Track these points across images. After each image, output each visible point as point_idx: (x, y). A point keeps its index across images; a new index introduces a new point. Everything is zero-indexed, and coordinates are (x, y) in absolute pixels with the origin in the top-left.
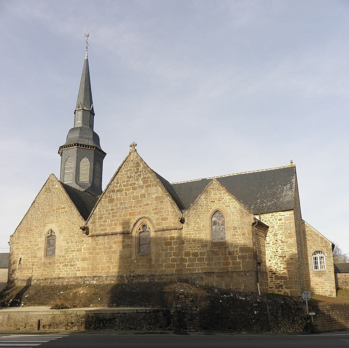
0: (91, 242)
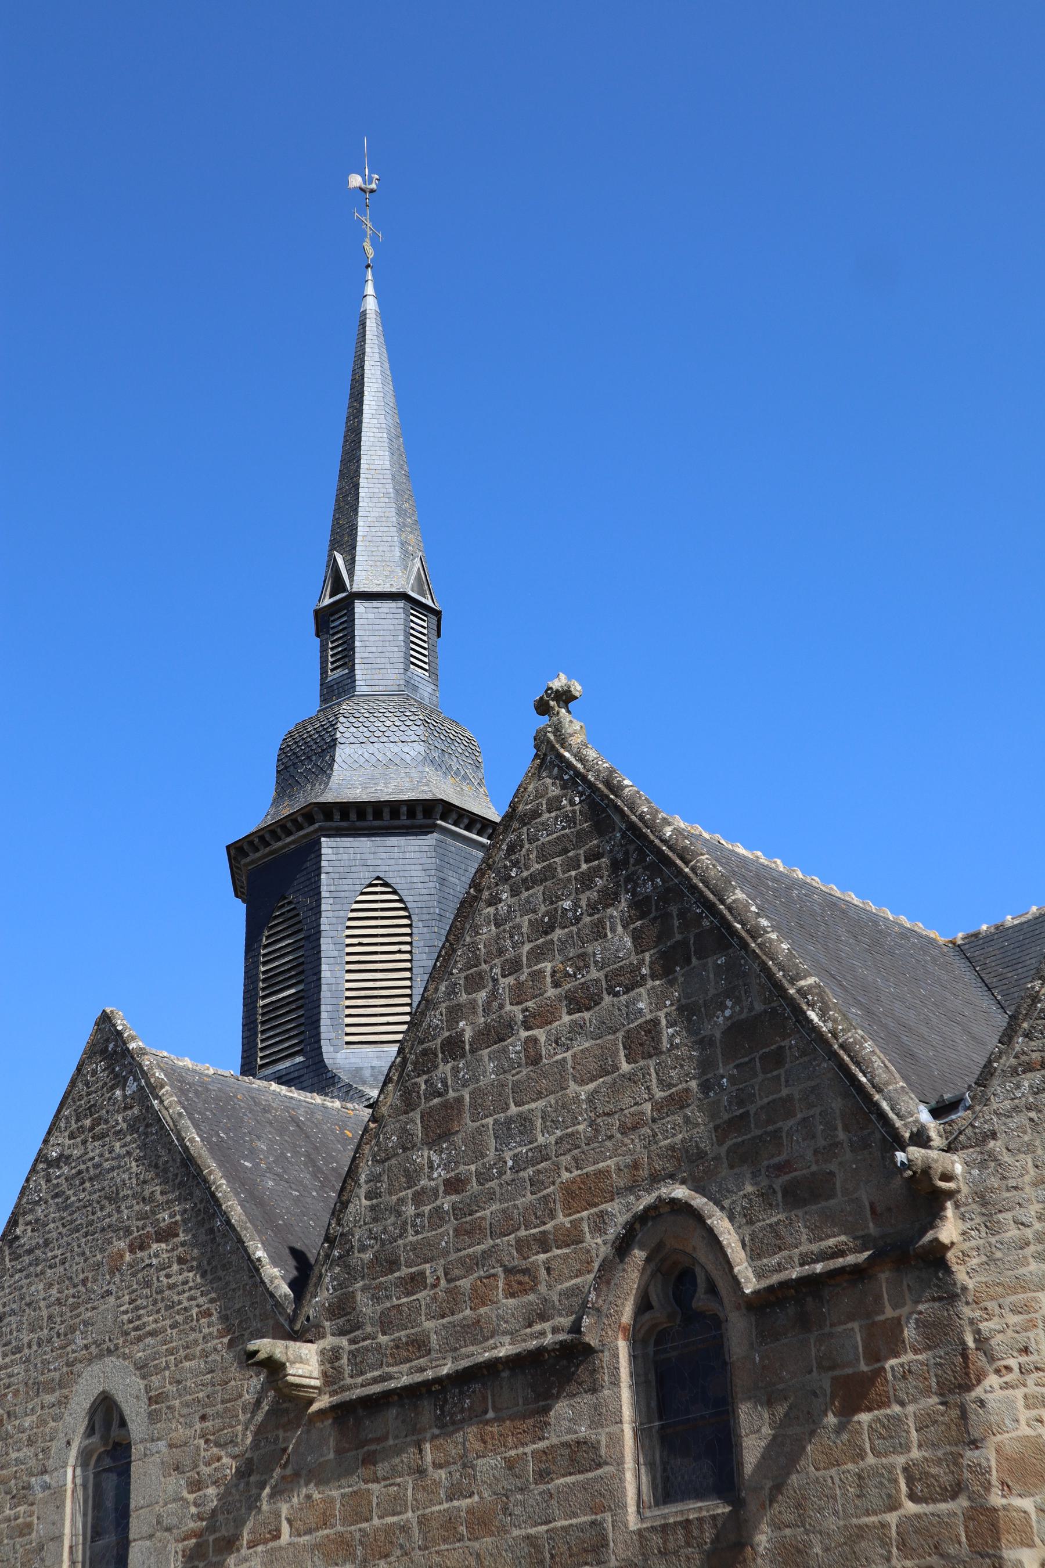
0: (332, 1456)
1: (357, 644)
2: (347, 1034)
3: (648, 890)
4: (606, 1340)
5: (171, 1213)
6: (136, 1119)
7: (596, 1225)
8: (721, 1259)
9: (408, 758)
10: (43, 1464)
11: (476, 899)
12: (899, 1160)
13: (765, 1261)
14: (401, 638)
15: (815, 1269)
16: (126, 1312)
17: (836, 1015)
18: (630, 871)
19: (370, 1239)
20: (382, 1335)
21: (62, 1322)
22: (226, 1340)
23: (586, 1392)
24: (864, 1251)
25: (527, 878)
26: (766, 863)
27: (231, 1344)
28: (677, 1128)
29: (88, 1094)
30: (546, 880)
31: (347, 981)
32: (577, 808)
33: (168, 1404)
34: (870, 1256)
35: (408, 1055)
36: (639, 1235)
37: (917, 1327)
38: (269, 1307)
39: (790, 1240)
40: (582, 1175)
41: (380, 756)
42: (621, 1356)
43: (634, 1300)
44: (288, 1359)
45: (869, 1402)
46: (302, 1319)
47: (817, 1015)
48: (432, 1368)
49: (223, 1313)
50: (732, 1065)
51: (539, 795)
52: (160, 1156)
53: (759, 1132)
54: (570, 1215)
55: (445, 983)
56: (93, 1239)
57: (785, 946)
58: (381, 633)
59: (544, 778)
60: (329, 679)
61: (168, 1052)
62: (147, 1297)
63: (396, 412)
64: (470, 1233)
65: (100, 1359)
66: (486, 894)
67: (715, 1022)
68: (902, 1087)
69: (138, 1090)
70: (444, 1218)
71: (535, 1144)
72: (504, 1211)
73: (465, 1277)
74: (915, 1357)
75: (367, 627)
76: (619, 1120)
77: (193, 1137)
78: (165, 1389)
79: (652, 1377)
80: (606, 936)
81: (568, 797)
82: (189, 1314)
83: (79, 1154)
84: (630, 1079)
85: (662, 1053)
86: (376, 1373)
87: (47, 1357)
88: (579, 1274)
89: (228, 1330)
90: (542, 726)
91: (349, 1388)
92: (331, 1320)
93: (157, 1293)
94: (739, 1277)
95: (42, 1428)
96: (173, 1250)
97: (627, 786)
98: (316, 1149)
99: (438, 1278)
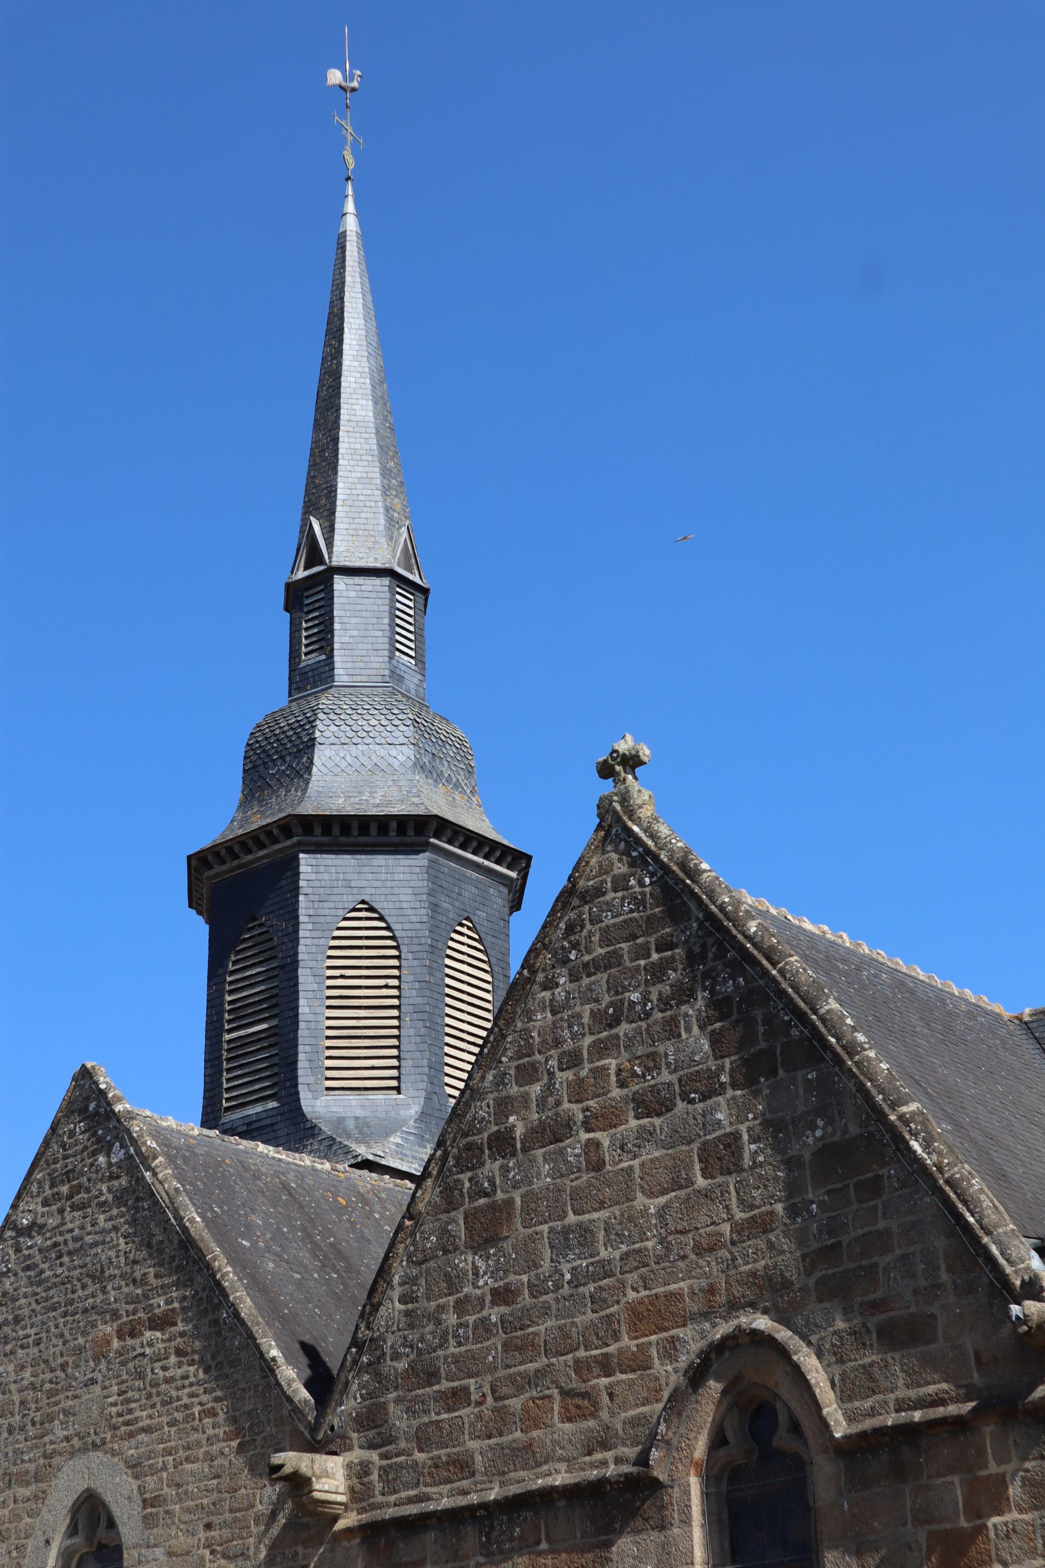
1: (336, 626)
2: (327, 1079)
3: (729, 990)
4: (676, 1476)
5: (167, 1300)
6: (124, 1191)
7: (666, 1351)
8: (807, 1398)
9: (396, 764)
10: (18, 1563)
11: (530, 981)
12: (822, 1122)
13: (857, 1404)
14: (386, 621)
15: (913, 1416)
16: (115, 1404)
17: (942, 1147)
18: (708, 967)
19: (405, 1346)
20: (419, 1452)
21: (38, 1410)
22: (234, 1444)
23: (653, 1529)
24: (968, 1401)
25: (588, 963)
26: (833, 938)
27: (241, 1449)
28: (759, 1253)
29: (65, 1157)
30: (611, 967)
31: (328, 1018)
32: (647, 889)
33: (167, 1508)
34: (974, 1409)
35: (449, 1149)
36: (715, 1366)
37: (1024, 1485)
38: (285, 1412)
39: (884, 1384)
40: (651, 1295)
41: (365, 760)
42: (693, 1493)
43: (709, 1435)
44: (314, 1474)
45: (968, 1560)
46: (325, 1427)
47: (921, 1145)
48: (476, 1491)
49: (231, 1413)
50: (822, 1191)
51: (604, 870)
52: (153, 1235)
53: (852, 1266)
54: (636, 1338)
55: (493, 1072)
56: (74, 1321)
57: (884, 1066)
58: (364, 614)
59: (608, 852)
60: (303, 664)
61: (151, 1111)
62: (139, 1390)
63: (380, 353)
64: (521, 1349)
65: (84, 1454)
66: (540, 977)
67: (805, 1142)
68: (1013, 1230)
69: (126, 1159)
70: (491, 1331)
71: (597, 1258)
72: (561, 1328)
73: (516, 1396)
74: (1020, 1517)
75: (347, 607)
76: (693, 1239)
77: (194, 1218)
78: (162, 1492)
79: (725, 1516)
80: (679, 1035)
81: (637, 877)
82: (190, 1412)
83: (55, 1224)
84: (706, 1196)
85: (743, 1170)
86: (412, 1493)
87: (21, 1446)
88: (646, 1402)
89: (237, 1433)
90: (606, 793)
91: (380, 1506)
92: (358, 1431)
93: (151, 1386)
94: (828, 1420)
95: (16, 1524)
96: (170, 1340)
97: (705, 871)
98: (311, 1221)
99: (484, 1395)
